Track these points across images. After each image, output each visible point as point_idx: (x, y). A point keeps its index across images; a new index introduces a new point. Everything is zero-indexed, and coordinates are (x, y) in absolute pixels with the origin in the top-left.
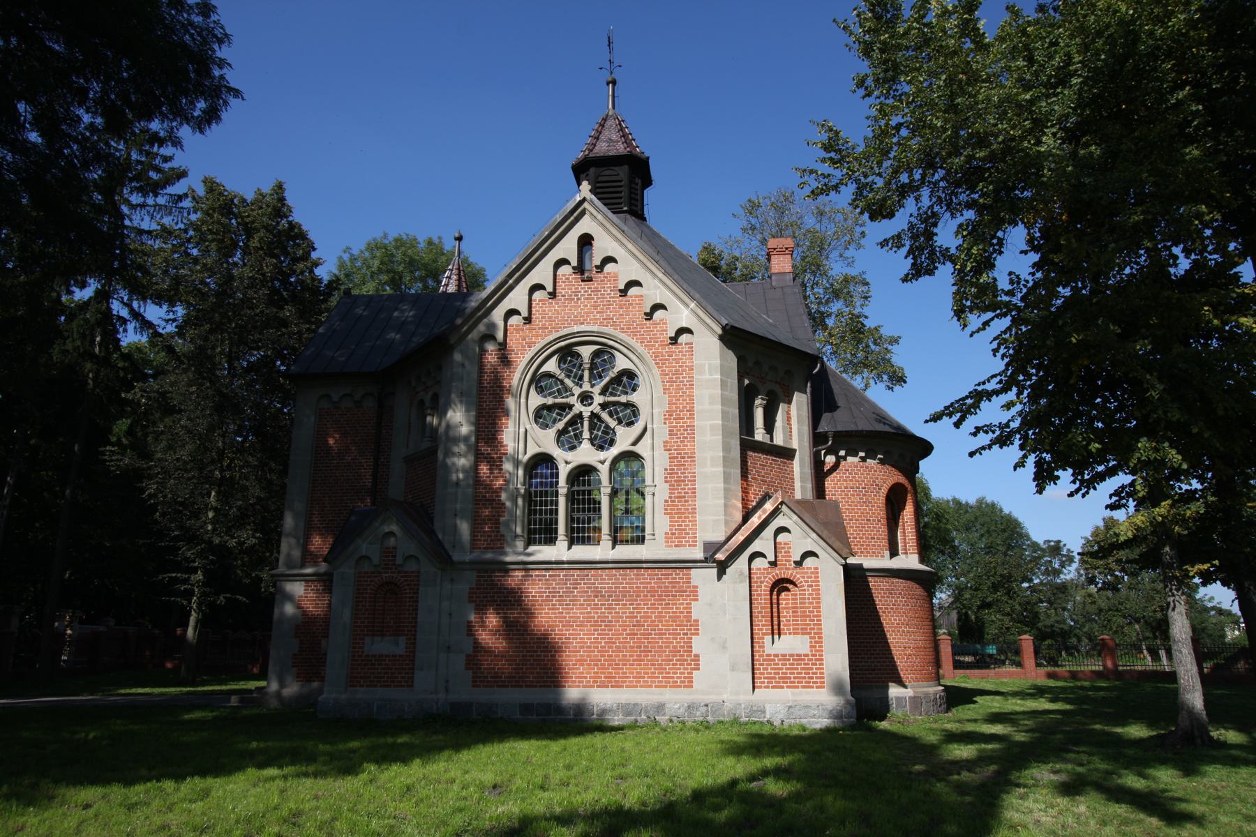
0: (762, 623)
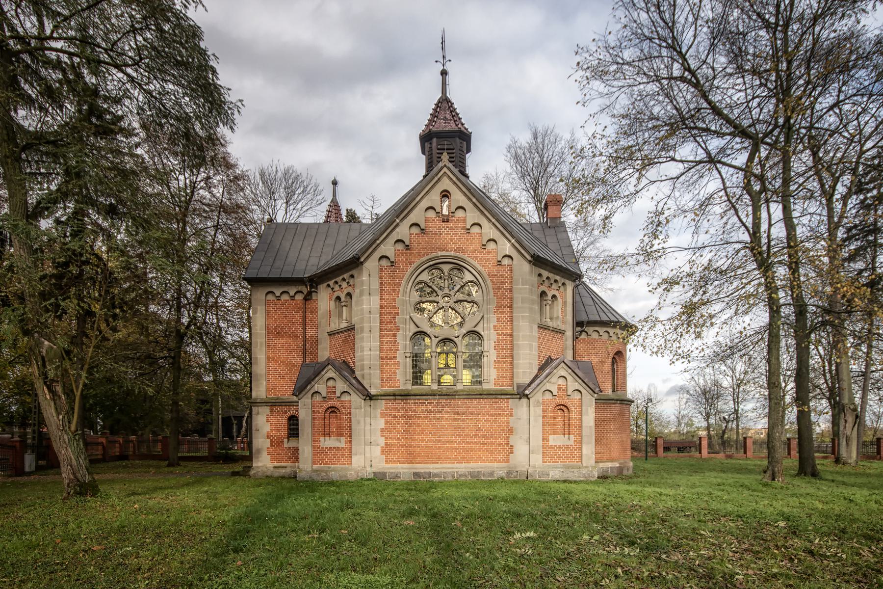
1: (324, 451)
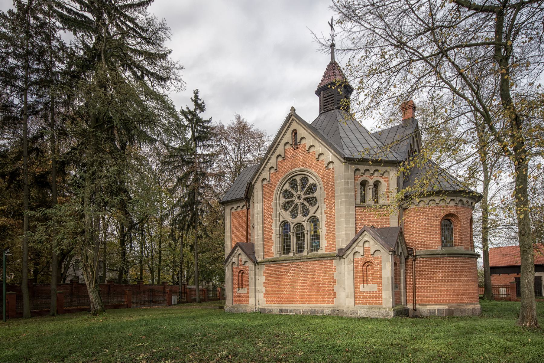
0: (359, 279)
1: (239, 296)
